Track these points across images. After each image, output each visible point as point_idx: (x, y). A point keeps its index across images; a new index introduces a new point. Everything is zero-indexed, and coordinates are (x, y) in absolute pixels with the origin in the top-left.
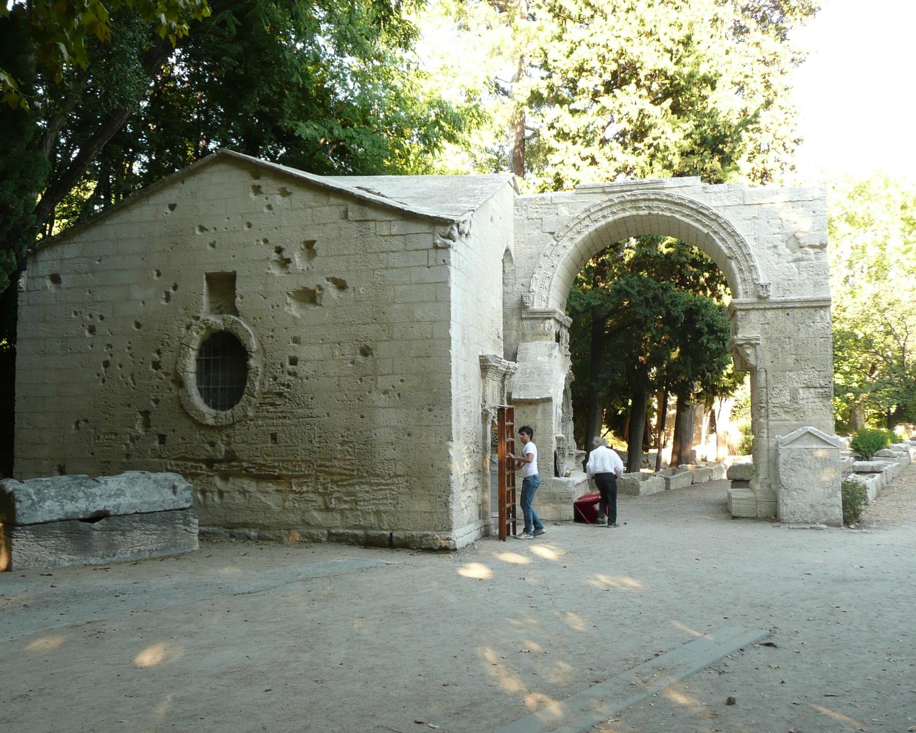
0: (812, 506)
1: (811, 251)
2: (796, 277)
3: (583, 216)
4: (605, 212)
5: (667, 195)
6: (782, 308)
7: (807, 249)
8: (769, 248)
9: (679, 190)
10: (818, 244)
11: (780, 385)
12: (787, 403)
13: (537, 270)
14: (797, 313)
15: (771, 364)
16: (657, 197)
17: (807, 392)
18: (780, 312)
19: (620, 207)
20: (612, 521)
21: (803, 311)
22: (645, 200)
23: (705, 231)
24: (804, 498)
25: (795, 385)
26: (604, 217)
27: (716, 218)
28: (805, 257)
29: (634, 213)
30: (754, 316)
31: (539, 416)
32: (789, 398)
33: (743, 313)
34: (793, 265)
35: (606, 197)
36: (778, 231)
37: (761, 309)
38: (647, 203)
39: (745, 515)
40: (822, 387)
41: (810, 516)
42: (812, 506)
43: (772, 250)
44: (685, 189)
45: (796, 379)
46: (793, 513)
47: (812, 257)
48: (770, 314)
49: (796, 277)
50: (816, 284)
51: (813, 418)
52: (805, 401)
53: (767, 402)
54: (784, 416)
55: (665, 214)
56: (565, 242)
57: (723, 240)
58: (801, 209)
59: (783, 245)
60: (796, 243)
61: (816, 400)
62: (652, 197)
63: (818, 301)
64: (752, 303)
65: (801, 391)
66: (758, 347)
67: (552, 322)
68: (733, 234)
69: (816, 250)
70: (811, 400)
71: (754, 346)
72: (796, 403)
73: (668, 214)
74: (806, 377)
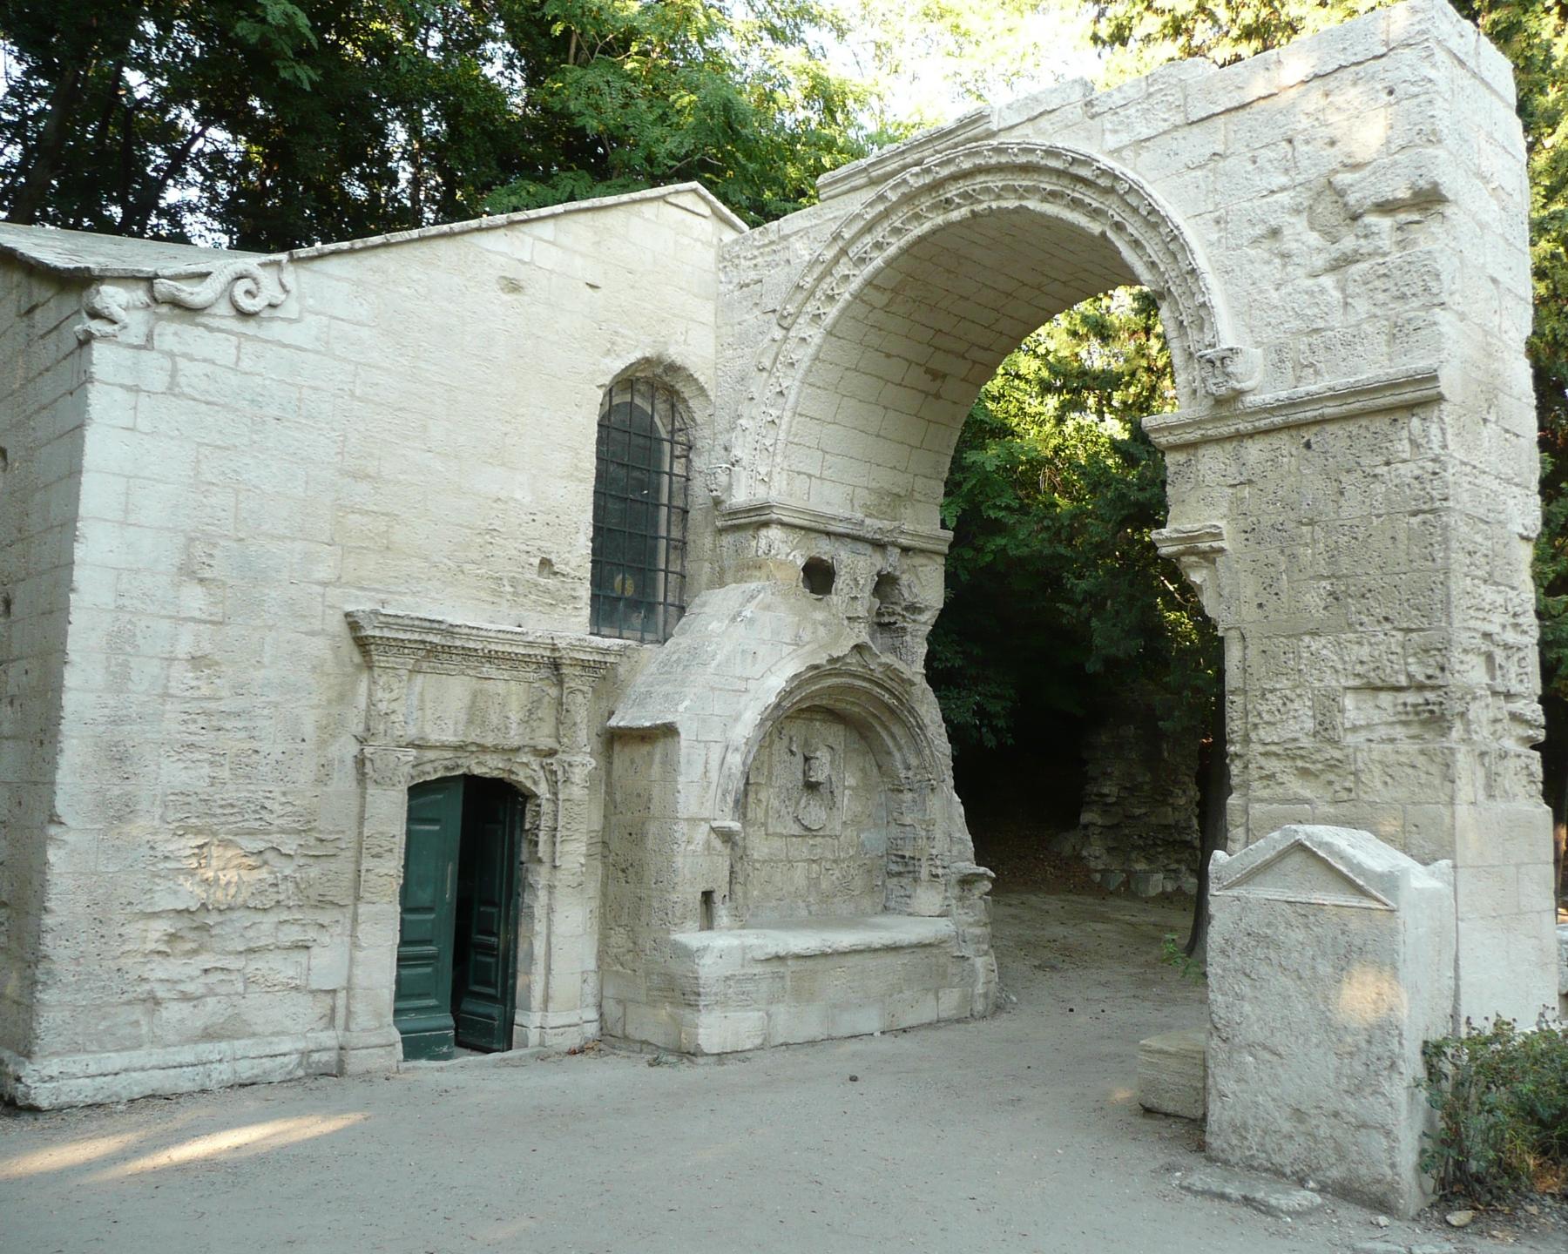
0: (1299, 1115)
1: (1384, 223)
2: (1337, 319)
3: (829, 255)
4: (879, 234)
5: (998, 150)
6: (1287, 427)
7: (1370, 219)
8: (1255, 241)
9: (1028, 129)
10: (1403, 193)
11: (1283, 683)
12: (1306, 742)
13: (744, 408)
14: (1334, 439)
15: (1256, 614)
16: (979, 161)
17: (1368, 700)
18: (1284, 442)
19: (906, 211)
20: (1426, 1043)
21: (1352, 427)
22: (954, 178)
23: (1096, 228)
24: (1275, 1079)
25: (1331, 681)
26: (878, 246)
27: (1109, 184)
28: (1366, 246)
29: (940, 220)
30: (1211, 462)
31: (656, 770)
32: (1310, 725)
33: (1181, 457)
34: (1328, 281)
35: (869, 194)
36: (1283, 180)
37: (1230, 438)
38: (963, 186)
39: (1170, 1107)
40: (1421, 688)
41: (1291, 1149)
42: (1299, 1115)
43: (1266, 244)
44: (1043, 122)
45: (1331, 660)
46: (1240, 1130)
47: (1386, 243)
48: (1254, 451)
49: (1337, 319)
50: (1398, 333)
51: (1387, 794)
52: (1361, 737)
53: (1247, 740)
54: (1296, 786)
55: (1004, 204)
56: (803, 328)
57: (1136, 244)
58: (1353, 93)
59: (1301, 223)
60: (1335, 206)
61: (1399, 732)
62: (967, 165)
63: (1393, 386)
64: (1197, 423)
65: (1349, 701)
66: (1220, 560)
67: (775, 533)
68: (1154, 219)
69: (1403, 217)
70: (1383, 732)
71: (1210, 557)
72: (1334, 742)
73: (1011, 204)
74: (1364, 652)
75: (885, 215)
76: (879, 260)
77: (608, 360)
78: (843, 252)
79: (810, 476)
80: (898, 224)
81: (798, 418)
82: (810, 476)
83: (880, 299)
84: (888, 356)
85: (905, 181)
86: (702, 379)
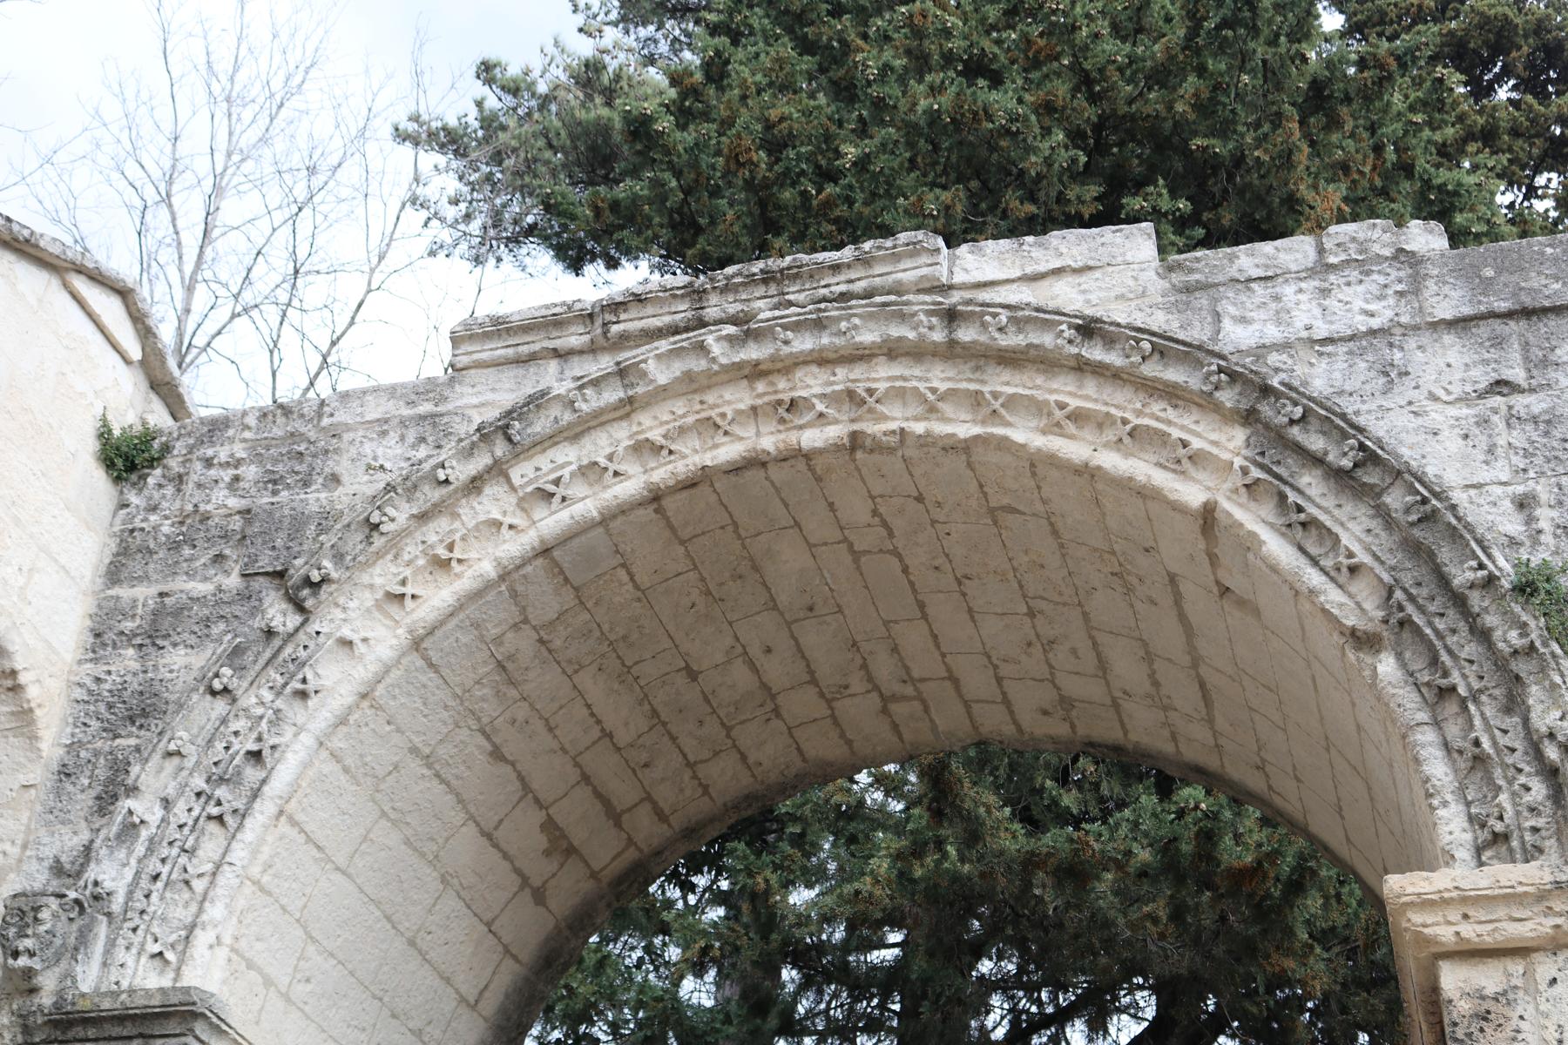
4: (598, 446)
16: (896, 331)
29: (769, 441)
33: (1489, 977)
75: (628, 408)
76: (587, 504)
78: (497, 470)
79: (268, 982)
80: (656, 435)
81: (284, 826)
82: (268, 982)
83: (547, 601)
84: (497, 754)
85: (701, 348)
86: (33, 692)
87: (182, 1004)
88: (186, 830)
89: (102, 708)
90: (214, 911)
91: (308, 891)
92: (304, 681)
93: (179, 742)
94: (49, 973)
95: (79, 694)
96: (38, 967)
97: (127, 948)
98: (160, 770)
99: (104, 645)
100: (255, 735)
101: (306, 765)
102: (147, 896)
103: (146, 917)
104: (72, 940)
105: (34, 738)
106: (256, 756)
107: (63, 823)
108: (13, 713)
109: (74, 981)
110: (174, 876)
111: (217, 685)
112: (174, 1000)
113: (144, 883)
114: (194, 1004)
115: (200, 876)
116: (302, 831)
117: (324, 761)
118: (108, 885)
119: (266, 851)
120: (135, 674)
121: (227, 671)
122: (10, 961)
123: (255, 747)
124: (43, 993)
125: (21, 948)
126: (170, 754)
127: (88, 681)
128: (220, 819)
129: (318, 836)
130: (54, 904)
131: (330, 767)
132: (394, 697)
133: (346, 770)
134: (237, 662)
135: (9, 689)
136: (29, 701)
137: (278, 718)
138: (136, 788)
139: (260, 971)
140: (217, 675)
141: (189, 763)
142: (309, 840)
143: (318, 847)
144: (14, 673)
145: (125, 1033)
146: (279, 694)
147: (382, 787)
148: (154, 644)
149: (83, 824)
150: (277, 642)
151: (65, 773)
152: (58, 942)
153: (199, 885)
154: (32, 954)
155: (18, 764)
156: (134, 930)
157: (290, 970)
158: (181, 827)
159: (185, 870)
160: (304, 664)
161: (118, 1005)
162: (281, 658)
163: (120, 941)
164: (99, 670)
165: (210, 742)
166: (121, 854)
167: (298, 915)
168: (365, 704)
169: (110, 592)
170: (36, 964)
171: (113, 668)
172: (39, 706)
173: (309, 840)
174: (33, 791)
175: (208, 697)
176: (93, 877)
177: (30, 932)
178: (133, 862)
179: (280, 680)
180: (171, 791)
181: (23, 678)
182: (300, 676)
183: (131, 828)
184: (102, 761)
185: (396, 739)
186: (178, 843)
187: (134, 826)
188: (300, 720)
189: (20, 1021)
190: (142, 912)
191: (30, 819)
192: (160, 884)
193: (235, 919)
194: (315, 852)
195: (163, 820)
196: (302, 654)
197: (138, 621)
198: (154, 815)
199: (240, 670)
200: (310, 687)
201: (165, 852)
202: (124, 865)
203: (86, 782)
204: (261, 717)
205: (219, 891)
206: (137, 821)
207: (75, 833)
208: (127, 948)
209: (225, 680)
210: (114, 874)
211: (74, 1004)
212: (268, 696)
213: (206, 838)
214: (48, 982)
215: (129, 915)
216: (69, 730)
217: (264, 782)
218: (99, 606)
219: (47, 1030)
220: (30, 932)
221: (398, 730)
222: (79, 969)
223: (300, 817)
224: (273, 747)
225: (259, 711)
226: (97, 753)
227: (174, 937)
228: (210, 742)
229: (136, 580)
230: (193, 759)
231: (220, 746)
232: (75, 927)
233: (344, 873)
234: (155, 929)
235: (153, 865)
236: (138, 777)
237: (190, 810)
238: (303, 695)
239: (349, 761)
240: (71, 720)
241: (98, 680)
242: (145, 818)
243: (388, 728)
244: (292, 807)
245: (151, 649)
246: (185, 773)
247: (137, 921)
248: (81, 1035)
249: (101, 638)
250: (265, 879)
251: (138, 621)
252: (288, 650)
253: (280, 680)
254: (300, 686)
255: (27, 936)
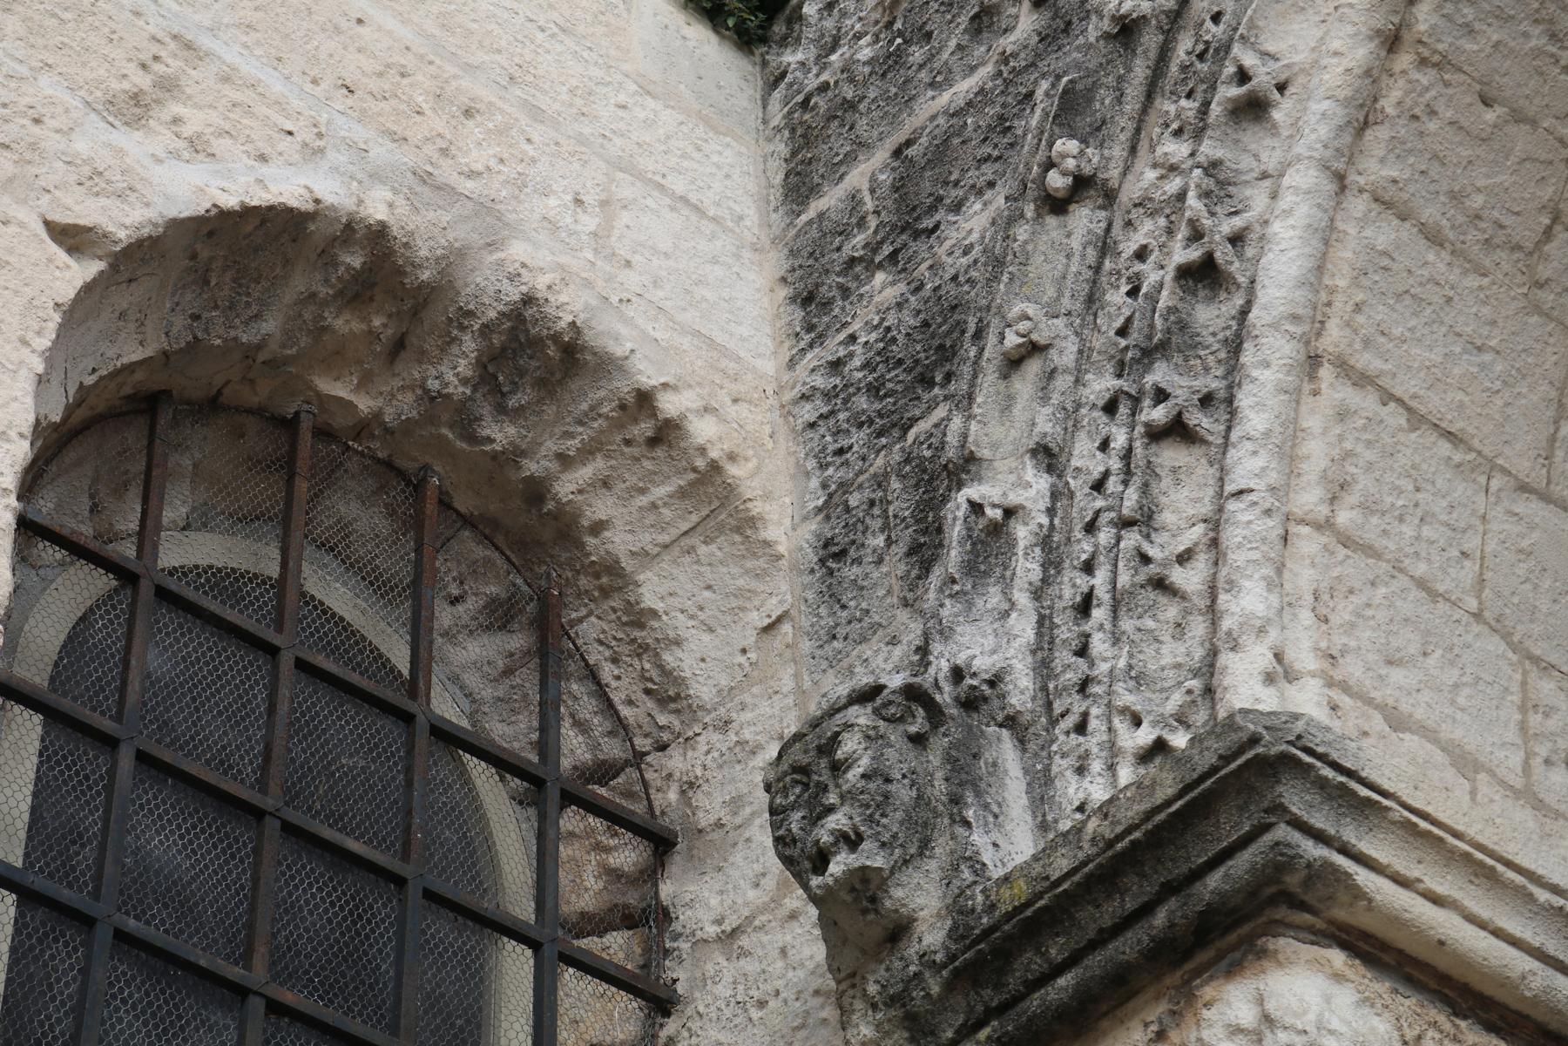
77: (135, 147)
86: (702, 430)
87: (1226, 759)
88: (1113, 485)
89: (862, 402)
90: (1248, 600)
91: (1472, 543)
92: (1243, 76)
93: (1023, 326)
94: (912, 877)
95: (808, 412)
96: (879, 862)
97: (1081, 771)
98: (1008, 402)
99: (826, 305)
100: (1182, 233)
101: (1327, 235)
102: (1082, 651)
103: (1096, 689)
104: (939, 788)
105: (746, 524)
106: (1204, 275)
107: (864, 639)
108: (682, 493)
109: (979, 868)
110: (1124, 579)
111: (1057, 181)
112: (1210, 759)
113: (1066, 631)
114: (1254, 740)
115: (1184, 558)
116: (1387, 397)
117: (1363, 222)
118: (984, 664)
119: (1316, 453)
120: (899, 306)
121: (1067, 146)
122: (815, 881)
123: (1194, 254)
124: (920, 927)
125: (826, 839)
126: (1013, 363)
127: (819, 381)
128: (1178, 430)
129: (1434, 403)
130: (861, 716)
131: (1386, 233)
132: (1469, 31)
133: (1433, 237)
134: (1083, 123)
135: (653, 442)
136: (702, 450)
137: (1220, 184)
138: (971, 459)
139: (1427, 733)
140: (1049, 165)
141: (1065, 354)
142: (1416, 419)
143: (1449, 435)
144: (645, 399)
145: (1130, 905)
146: (1198, 135)
147: (1544, 271)
148: (917, 235)
149: (903, 615)
150: (1150, 40)
151: (833, 554)
152: (903, 793)
153: (1189, 579)
154: (852, 841)
155: (739, 593)
156: (1081, 728)
157: (1512, 735)
158: (1098, 486)
159: (1145, 559)
160: (1227, 47)
161: (1088, 849)
162: (1174, 68)
163: (1059, 764)
164: (833, 347)
165: (1092, 300)
166: (993, 597)
167: (1472, 604)
168: (1404, 60)
169: (811, 213)
170: (873, 857)
171: (856, 326)
172: (732, 457)
173: (1416, 419)
174: (786, 628)
175: (1052, 221)
176: (945, 665)
177: (832, 798)
178: (1022, 598)
179: (1189, 106)
180: (1046, 425)
181: (669, 405)
182: (1230, 69)
183: (992, 536)
184: (895, 484)
185: (1522, 140)
186: (1105, 517)
187: (996, 529)
188: (1270, 161)
189: (895, 1012)
190: (1084, 686)
191: (797, 676)
192: (1099, 614)
193: (1306, 617)
194: (1445, 448)
195: (1055, 495)
196: (1214, 31)
197: (873, 222)
198: (1034, 488)
199: (1095, 133)
200: (1263, 77)
201: (1085, 548)
202: (1005, 615)
203: (880, 541)
204: (1181, 196)
205: (1237, 557)
206: (996, 514)
207: (893, 641)
208: (1081, 771)
209: (1070, 163)
210: (990, 642)
211: (992, 907)
212: (1177, 150)
213: (1166, 482)
214: (922, 897)
215: (1058, 708)
216: (814, 483)
217: (1244, 312)
218: (793, 253)
219: (959, 1000)
220: (832, 798)
221: (1518, 117)
222: (978, 838)
223: (1366, 361)
224: (1236, 239)
225: (1173, 185)
226: (880, 482)
227: (1176, 699)
228: (1092, 300)
229: (837, 169)
230: (1071, 347)
231: (1116, 297)
232: (934, 758)
233: (1545, 497)
234: (1125, 697)
235: (1070, 586)
236: (965, 436)
237: (1104, 446)
238: (1253, 109)
239: (1544, 157)
240: (811, 464)
241: (836, 365)
242: (1014, 499)
243: (1490, 116)
244: (1334, 337)
245: (920, 246)
246: (1063, 382)
247: (1078, 706)
248: (1038, 965)
249: (812, 300)
250: (1345, 517)
251: (873, 222)
252: (1184, 45)
253: (1189, 106)
254: (1234, 91)
255: (831, 809)
